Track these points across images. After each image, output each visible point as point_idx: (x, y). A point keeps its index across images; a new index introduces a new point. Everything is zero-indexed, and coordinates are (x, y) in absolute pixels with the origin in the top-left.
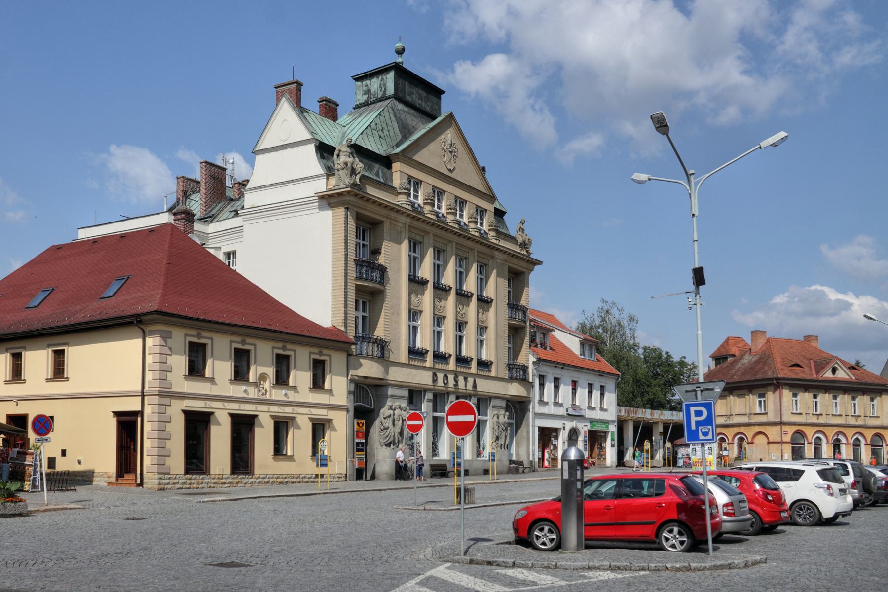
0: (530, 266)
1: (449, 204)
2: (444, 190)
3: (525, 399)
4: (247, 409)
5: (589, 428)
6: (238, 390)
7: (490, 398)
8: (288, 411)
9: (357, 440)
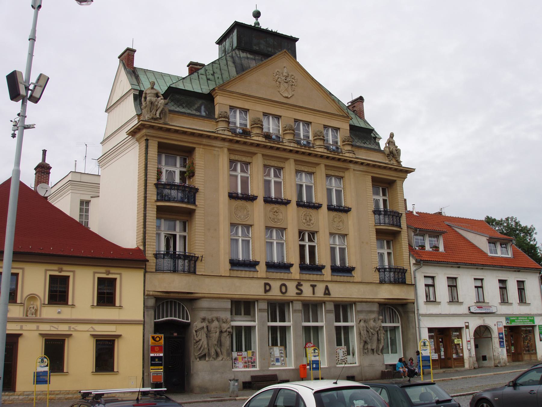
0: (401, 175)
1: (285, 126)
2: (310, 121)
3: (405, 301)
5: (505, 324)
7: (355, 303)
8: (63, 329)
9: (152, 355)
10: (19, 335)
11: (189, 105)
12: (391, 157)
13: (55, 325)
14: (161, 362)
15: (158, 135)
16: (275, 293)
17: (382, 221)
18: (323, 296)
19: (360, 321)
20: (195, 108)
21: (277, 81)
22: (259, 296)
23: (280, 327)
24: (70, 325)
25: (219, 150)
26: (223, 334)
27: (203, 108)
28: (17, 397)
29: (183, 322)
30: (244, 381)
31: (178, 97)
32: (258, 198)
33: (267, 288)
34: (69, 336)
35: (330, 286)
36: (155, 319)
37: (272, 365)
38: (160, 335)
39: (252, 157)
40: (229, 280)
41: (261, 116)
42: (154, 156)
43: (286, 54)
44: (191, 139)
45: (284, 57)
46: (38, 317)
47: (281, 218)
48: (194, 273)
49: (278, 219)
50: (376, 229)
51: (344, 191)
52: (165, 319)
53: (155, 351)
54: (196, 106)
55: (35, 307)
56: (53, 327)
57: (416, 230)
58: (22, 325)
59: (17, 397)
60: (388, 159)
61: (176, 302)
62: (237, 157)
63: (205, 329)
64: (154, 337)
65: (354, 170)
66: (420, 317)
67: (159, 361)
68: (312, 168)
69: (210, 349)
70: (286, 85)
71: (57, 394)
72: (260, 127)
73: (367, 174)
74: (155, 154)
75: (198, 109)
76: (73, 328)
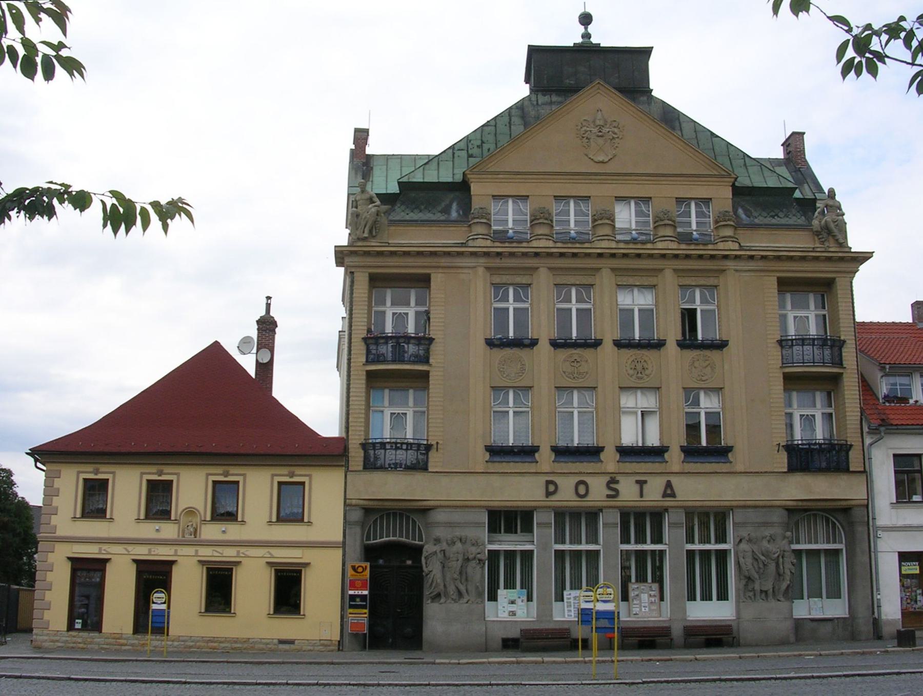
0: (843, 266)
3: (844, 503)
4: (162, 553)
6: (150, 530)
8: (229, 554)
9: (351, 592)
10: (173, 563)
11: (430, 205)
12: (825, 235)
13: (219, 549)
14: (365, 603)
15: (719, 267)
16: (566, 495)
17: (817, 358)
18: (661, 499)
19: (741, 541)
20: (440, 208)
21: (583, 137)
22: (528, 502)
24: (238, 549)
25: (470, 271)
26: (470, 563)
27: (454, 206)
28: (170, 643)
29: (414, 544)
30: (504, 637)
31: (413, 195)
32: (539, 343)
33: (551, 488)
34: (238, 563)
36: (368, 539)
37: (635, 614)
38: (364, 564)
39: (532, 275)
40: (483, 479)
41: (672, 207)
42: (363, 295)
43: (601, 87)
44: (420, 261)
45: (599, 93)
46: (198, 538)
47: (586, 370)
49: (580, 373)
50: (784, 373)
51: (718, 311)
52: (385, 539)
53: (355, 587)
54: (443, 205)
55: (194, 525)
56: (216, 551)
57: (884, 368)
58: (177, 548)
59: (170, 643)
60: (819, 239)
61: (403, 514)
62: (505, 279)
63: (440, 556)
64: (355, 566)
65: (736, 271)
66: (879, 532)
67: (361, 601)
68: (651, 279)
69: (448, 586)
70: (600, 141)
71: (221, 642)
72: (672, 225)
73: (767, 274)
74: (364, 293)
75: (447, 210)
76: (243, 553)
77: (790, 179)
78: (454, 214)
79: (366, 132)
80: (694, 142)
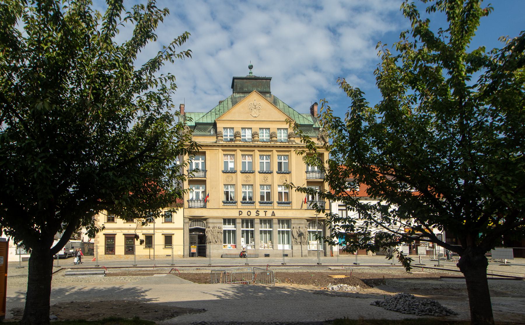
8: (151, 232)
11: (205, 130)
13: (149, 230)
16: (245, 215)
23: (246, 230)
27: (212, 130)
33: (240, 213)
35: (275, 211)
36: (190, 227)
48: (206, 208)
75: (210, 132)
77: (312, 122)
78: (212, 133)
79: (265, 255)
80: (283, 110)
